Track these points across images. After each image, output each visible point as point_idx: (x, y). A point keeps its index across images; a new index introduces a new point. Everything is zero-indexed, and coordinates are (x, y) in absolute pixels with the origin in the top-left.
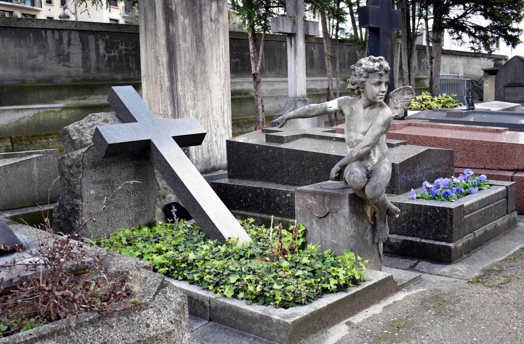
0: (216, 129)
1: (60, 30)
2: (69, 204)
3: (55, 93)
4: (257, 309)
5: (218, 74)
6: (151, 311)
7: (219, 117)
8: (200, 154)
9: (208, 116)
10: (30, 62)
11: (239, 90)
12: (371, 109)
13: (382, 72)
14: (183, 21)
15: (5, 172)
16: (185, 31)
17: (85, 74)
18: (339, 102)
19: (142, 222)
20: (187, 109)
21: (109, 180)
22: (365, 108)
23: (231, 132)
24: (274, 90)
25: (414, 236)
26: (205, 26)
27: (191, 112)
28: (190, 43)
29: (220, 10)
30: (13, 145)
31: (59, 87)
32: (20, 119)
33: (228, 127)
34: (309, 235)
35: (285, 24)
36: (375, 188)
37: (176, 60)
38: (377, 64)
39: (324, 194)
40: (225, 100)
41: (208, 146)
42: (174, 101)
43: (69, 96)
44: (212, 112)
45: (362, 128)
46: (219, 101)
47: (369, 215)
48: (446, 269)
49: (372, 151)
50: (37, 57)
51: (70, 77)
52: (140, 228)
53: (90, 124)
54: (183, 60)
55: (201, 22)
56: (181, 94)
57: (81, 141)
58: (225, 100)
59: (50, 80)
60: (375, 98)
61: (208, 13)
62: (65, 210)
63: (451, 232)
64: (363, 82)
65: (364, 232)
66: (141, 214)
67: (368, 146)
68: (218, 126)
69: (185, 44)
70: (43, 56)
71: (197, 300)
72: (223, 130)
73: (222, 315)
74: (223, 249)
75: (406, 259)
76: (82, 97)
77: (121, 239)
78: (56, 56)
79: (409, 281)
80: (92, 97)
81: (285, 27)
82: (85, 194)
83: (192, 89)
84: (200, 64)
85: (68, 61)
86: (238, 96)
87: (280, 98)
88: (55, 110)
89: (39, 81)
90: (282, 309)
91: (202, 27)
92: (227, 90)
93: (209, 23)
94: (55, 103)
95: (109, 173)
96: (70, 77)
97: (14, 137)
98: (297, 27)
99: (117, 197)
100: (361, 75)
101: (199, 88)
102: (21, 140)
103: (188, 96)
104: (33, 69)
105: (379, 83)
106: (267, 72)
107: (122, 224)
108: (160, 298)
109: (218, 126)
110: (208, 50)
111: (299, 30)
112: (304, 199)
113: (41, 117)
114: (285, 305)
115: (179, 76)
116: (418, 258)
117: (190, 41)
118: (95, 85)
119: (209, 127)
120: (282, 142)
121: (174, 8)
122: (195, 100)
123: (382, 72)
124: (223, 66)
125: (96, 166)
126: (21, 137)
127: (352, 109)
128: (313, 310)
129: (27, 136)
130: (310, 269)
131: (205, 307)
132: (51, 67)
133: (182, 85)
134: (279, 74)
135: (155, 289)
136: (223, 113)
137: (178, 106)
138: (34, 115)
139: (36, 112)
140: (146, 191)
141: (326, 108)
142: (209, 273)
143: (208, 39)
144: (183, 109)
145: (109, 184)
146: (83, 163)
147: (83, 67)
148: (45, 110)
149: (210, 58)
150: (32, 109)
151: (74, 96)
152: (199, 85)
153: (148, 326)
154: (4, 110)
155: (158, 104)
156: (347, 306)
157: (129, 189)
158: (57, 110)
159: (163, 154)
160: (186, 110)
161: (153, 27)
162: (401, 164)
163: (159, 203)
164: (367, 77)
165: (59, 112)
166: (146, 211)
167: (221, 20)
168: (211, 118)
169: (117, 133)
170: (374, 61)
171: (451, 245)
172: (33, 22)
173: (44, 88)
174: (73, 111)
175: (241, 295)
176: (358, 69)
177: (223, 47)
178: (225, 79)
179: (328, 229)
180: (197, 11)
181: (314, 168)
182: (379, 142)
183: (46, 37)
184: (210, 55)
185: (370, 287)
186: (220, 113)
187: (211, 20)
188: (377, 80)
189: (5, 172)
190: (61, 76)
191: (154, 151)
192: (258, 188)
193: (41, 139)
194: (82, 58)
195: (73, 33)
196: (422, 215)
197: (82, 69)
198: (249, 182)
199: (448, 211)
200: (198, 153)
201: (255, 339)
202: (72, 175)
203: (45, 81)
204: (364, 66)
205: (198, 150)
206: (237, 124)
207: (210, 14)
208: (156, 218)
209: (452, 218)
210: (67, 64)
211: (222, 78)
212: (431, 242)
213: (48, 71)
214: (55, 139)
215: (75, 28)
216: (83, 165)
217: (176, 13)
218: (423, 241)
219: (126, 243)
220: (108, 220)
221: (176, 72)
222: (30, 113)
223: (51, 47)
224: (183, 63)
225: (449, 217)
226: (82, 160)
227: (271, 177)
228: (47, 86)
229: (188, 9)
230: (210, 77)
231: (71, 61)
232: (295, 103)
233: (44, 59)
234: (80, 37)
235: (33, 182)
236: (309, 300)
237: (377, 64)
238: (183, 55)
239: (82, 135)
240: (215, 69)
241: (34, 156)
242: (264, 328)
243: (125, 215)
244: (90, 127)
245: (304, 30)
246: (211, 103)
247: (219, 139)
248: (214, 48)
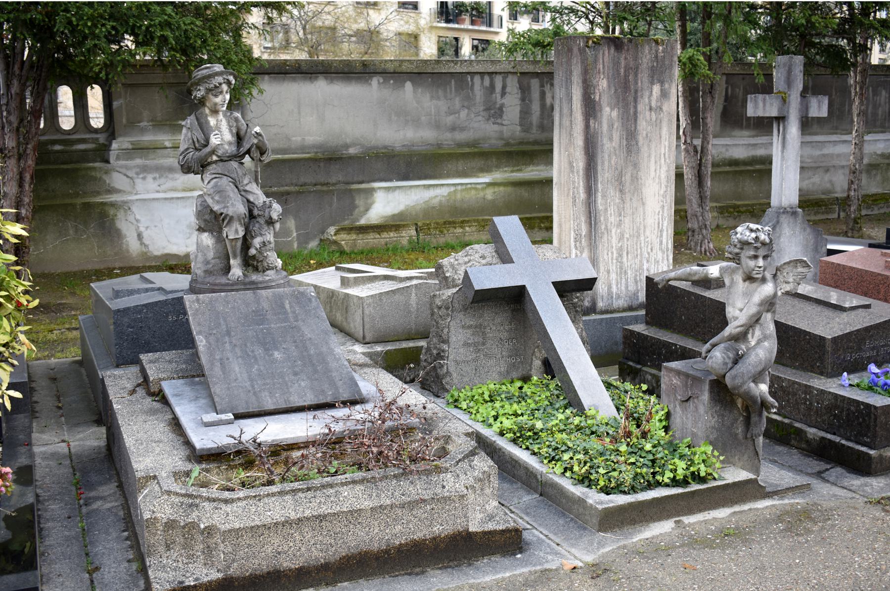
0: (649, 254)
1: (493, 73)
2: (435, 348)
3: (479, 163)
4: (578, 491)
5: (657, 180)
6: (449, 475)
7: (654, 237)
8: (623, 285)
9: (638, 236)
10: (450, 120)
11: (761, 156)
12: (751, 283)
13: (759, 245)
14: (609, 113)
15: (381, 300)
16: (611, 126)
17: (523, 134)
18: (721, 269)
19: (515, 375)
21: (481, 325)
22: (744, 281)
23: (671, 257)
24: (824, 155)
25: (834, 434)
26: (640, 117)
27: (614, 231)
28: (618, 141)
29: (664, 95)
30: (418, 235)
31: (485, 155)
32: (431, 199)
34: (672, 418)
35: (768, 105)
36: (734, 378)
37: (596, 164)
38: (753, 235)
39: (687, 376)
41: (636, 275)
42: (590, 218)
43: (498, 167)
44: (644, 231)
45: (739, 304)
47: (739, 406)
48: (857, 482)
49: (751, 331)
50: (459, 112)
51: (502, 139)
52: (512, 382)
53: (466, 259)
54: (606, 163)
55: (635, 113)
56: (600, 207)
57: (454, 280)
58: (666, 215)
59: (474, 144)
60: (750, 273)
61: (647, 100)
62: (431, 354)
63: (875, 436)
64: (737, 254)
65: (732, 424)
66: (514, 366)
67: (742, 326)
69: (610, 145)
70: (466, 111)
71: (532, 472)
72: (660, 254)
73: (550, 491)
74: (577, 420)
75: (821, 461)
76: (516, 168)
77: (483, 393)
78: (484, 110)
79: (787, 489)
80: (531, 168)
81: (767, 108)
82: (453, 339)
83: (617, 201)
84: (630, 168)
85: (501, 116)
86: (758, 167)
87: (832, 169)
88: (478, 186)
89: (460, 145)
90: (603, 495)
91: (636, 120)
92: (669, 201)
93: (648, 113)
94: (478, 177)
95: (480, 317)
96: (502, 139)
97: (420, 224)
98: (788, 108)
99: (488, 345)
100: (735, 246)
101: (628, 199)
102: (429, 229)
103: (611, 210)
104: (453, 129)
105: (756, 257)
106: (815, 126)
107: (491, 376)
108: (465, 465)
110: (644, 150)
111: (791, 111)
112: (669, 377)
113: (459, 196)
114: (606, 491)
115: (599, 185)
116: (836, 462)
117: (618, 139)
118: (535, 151)
120: (709, 288)
121: (597, 98)
122: (620, 215)
123: (759, 245)
124: (664, 168)
125: (467, 309)
126: (430, 224)
127: (733, 279)
128: (633, 500)
129: (437, 223)
130: (651, 457)
131: (537, 480)
132: (476, 125)
133: (604, 196)
134: (837, 128)
135: (460, 457)
136: (661, 231)
137: (595, 224)
138: (449, 194)
139: (452, 189)
140: (522, 340)
141: (707, 274)
142: (549, 446)
143: (644, 135)
144: (603, 227)
145: (479, 329)
147: (521, 125)
148: (464, 187)
149: (646, 160)
150: (448, 185)
151: (506, 166)
152: (628, 196)
153: (444, 487)
154: (411, 187)
156: (682, 503)
158: (479, 187)
159: (536, 304)
161: (568, 123)
162: (835, 340)
163: (538, 354)
164: (742, 249)
165: (483, 189)
166: (522, 362)
167: (665, 108)
168: (642, 238)
169: (491, 276)
170: (752, 231)
171: (872, 452)
172: (456, 64)
173: (464, 156)
174: (502, 188)
175: (568, 474)
176: (734, 239)
177: (667, 143)
178: (666, 187)
179: (689, 415)
180: (631, 99)
182: (761, 321)
183: (473, 85)
184: (646, 155)
185: (718, 487)
186: (656, 232)
187: (651, 109)
188: (752, 253)
189: (381, 300)
190: (490, 138)
191: (527, 299)
193: (455, 228)
194: (521, 112)
195: (510, 76)
197: (519, 128)
198: (667, 333)
201: (572, 519)
202: (441, 317)
203: (468, 145)
204: (738, 236)
206: (750, 212)
207: (650, 101)
208: (533, 371)
209: (876, 419)
210: (499, 121)
212: (850, 444)
213: (472, 131)
214: (474, 229)
215: (512, 70)
217: (600, 105)
218: (843, 442)
219: (488, 399)
221: (596, 181)
222: (444, 191)
223: (478, 97)
224: (606, 168)
225: (873, 416)
227: (692, 331)
228: (469, 153)
229: (618, 98)
231: (505, 117)
232: (778, 217)
233: (468, 115)
234: (519, 82)
235: (410, 312)
236: (633, 490)
237: (753, 235)
238: (606, 157)
239: (456, 273)
240: (653, 174)
241: (415, 282)
242: (581, 510)
244: (466, 263)
245: (800, 110)
246: (644, 219)
248: (653, 146)
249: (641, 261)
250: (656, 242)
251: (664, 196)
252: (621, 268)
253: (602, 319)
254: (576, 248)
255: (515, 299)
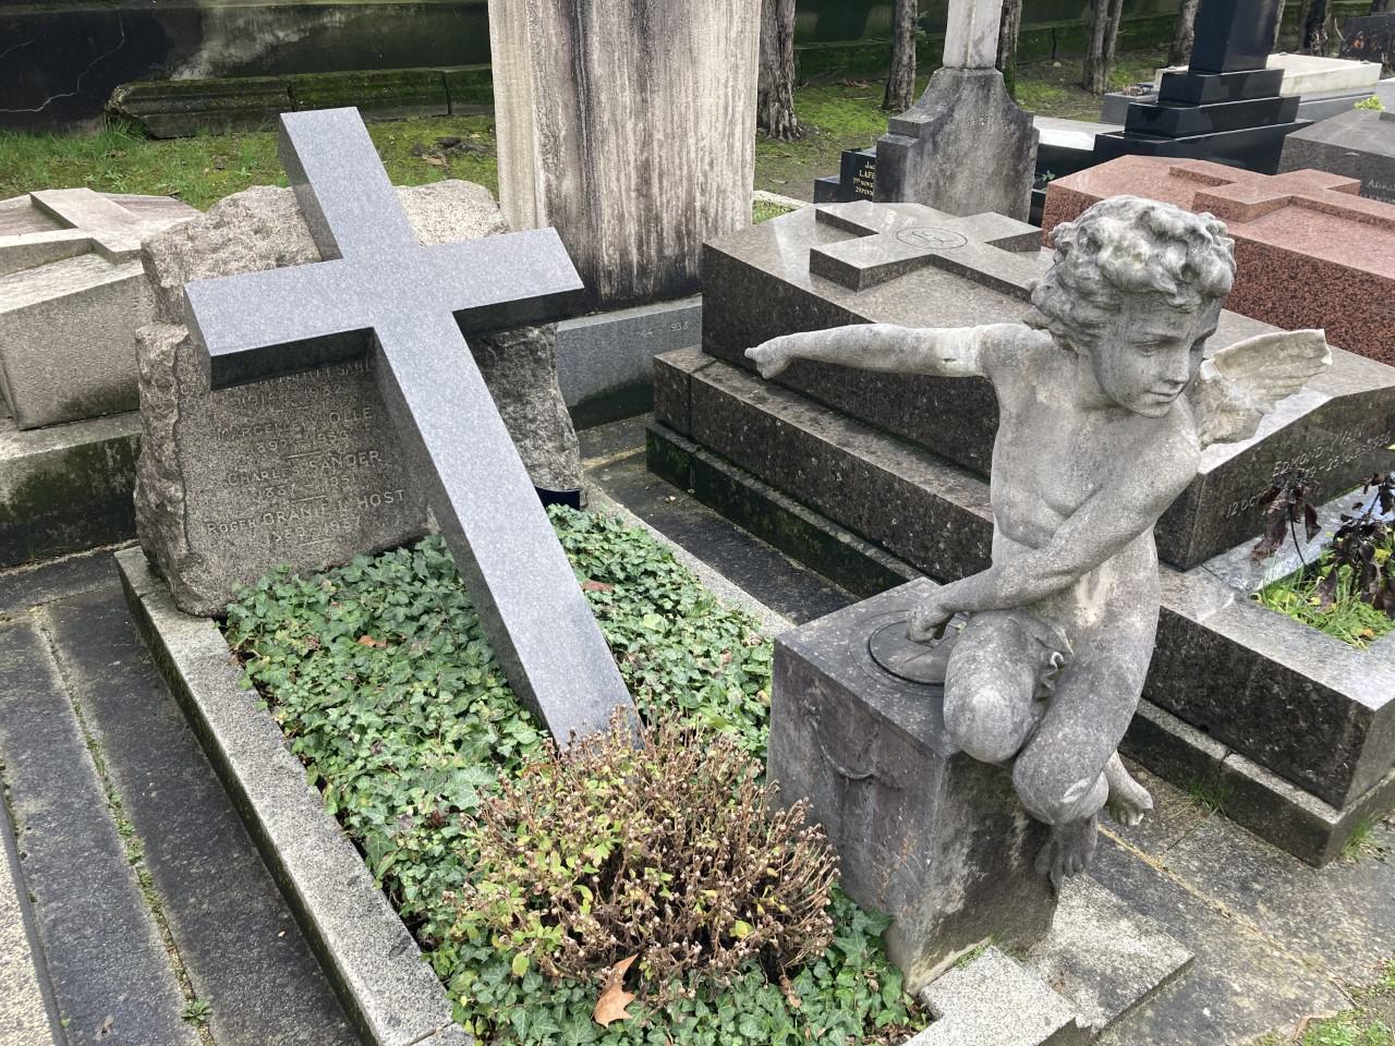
7: (716, 136)
8: (653, 246)
20: (619, 118)
27: (629, 126)
33: (743, 167)
38: (1173, 257)
40: (741, 87)
41: (680, 223)
44: (696, 123)
46: (721, 87)
58: (741, 87)
68: (711, 164)
82: (194, 467)
92: (748, 54)
99: (300, 472)
109: (711, 164)
115: (595, 16)
119: (685, 168)
136: (732, 123)
144: (606, 117)
146: (178, 378)
155: (528, 104)
157: (337, 447)
160: (613, 120)
168: (692, 141)
170: (1162, 236)
178: (744, 21)
181: (930, 400)
186: (720, 126)
192: (766, 415)
196: (1250, 684)
199: (1352, 713)
200: (648, 243)
205: (648, 238)
211: (736, 17)
216: (179, 382)
220: (273, 538)
226: (174, 368)
230: (697, 15)
237: (1173, 257)
243: (328, 522)
247: (714, 202)
249: (690, 193)
250: (720, 148)
251: (739, 43)
252: (648, 209)
253: (610, 326)
254: (547, 168)
255: (352, 359)
